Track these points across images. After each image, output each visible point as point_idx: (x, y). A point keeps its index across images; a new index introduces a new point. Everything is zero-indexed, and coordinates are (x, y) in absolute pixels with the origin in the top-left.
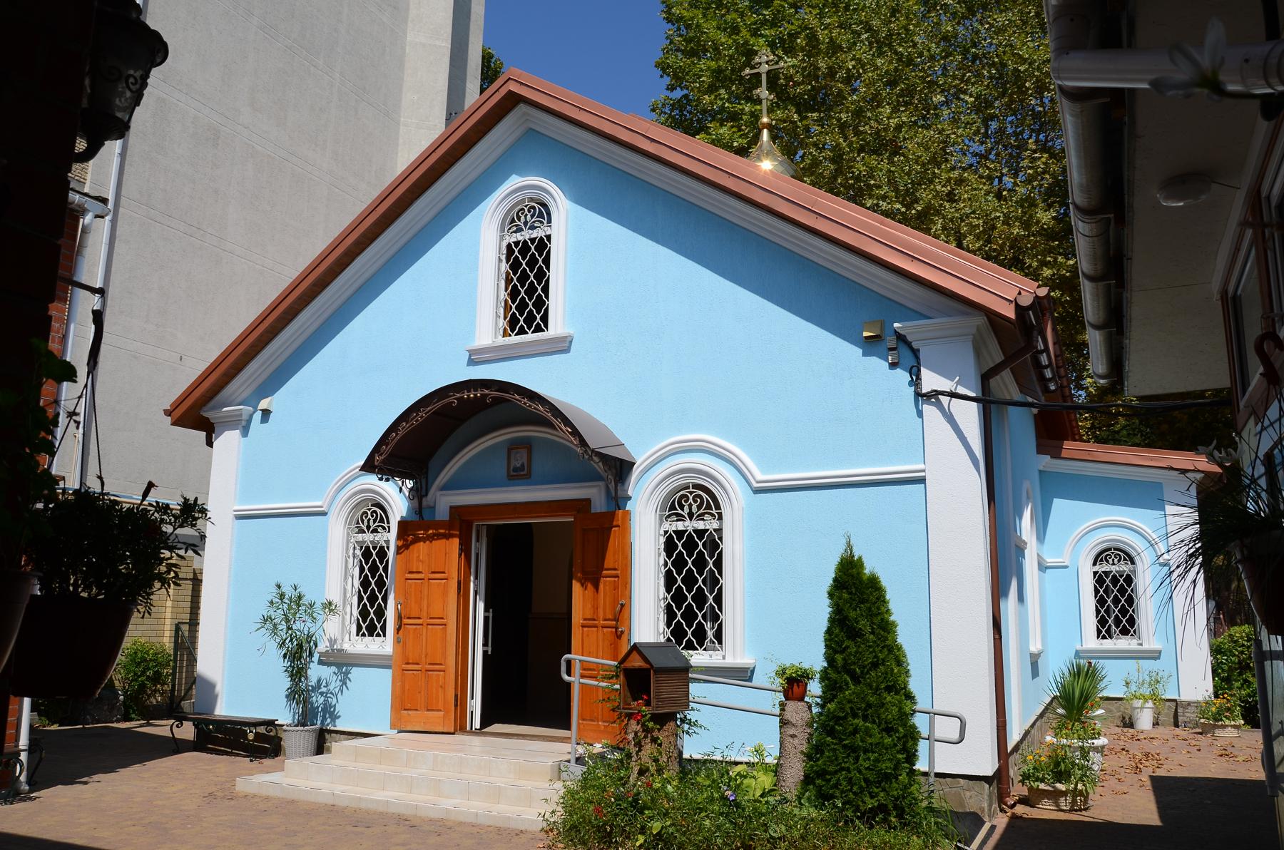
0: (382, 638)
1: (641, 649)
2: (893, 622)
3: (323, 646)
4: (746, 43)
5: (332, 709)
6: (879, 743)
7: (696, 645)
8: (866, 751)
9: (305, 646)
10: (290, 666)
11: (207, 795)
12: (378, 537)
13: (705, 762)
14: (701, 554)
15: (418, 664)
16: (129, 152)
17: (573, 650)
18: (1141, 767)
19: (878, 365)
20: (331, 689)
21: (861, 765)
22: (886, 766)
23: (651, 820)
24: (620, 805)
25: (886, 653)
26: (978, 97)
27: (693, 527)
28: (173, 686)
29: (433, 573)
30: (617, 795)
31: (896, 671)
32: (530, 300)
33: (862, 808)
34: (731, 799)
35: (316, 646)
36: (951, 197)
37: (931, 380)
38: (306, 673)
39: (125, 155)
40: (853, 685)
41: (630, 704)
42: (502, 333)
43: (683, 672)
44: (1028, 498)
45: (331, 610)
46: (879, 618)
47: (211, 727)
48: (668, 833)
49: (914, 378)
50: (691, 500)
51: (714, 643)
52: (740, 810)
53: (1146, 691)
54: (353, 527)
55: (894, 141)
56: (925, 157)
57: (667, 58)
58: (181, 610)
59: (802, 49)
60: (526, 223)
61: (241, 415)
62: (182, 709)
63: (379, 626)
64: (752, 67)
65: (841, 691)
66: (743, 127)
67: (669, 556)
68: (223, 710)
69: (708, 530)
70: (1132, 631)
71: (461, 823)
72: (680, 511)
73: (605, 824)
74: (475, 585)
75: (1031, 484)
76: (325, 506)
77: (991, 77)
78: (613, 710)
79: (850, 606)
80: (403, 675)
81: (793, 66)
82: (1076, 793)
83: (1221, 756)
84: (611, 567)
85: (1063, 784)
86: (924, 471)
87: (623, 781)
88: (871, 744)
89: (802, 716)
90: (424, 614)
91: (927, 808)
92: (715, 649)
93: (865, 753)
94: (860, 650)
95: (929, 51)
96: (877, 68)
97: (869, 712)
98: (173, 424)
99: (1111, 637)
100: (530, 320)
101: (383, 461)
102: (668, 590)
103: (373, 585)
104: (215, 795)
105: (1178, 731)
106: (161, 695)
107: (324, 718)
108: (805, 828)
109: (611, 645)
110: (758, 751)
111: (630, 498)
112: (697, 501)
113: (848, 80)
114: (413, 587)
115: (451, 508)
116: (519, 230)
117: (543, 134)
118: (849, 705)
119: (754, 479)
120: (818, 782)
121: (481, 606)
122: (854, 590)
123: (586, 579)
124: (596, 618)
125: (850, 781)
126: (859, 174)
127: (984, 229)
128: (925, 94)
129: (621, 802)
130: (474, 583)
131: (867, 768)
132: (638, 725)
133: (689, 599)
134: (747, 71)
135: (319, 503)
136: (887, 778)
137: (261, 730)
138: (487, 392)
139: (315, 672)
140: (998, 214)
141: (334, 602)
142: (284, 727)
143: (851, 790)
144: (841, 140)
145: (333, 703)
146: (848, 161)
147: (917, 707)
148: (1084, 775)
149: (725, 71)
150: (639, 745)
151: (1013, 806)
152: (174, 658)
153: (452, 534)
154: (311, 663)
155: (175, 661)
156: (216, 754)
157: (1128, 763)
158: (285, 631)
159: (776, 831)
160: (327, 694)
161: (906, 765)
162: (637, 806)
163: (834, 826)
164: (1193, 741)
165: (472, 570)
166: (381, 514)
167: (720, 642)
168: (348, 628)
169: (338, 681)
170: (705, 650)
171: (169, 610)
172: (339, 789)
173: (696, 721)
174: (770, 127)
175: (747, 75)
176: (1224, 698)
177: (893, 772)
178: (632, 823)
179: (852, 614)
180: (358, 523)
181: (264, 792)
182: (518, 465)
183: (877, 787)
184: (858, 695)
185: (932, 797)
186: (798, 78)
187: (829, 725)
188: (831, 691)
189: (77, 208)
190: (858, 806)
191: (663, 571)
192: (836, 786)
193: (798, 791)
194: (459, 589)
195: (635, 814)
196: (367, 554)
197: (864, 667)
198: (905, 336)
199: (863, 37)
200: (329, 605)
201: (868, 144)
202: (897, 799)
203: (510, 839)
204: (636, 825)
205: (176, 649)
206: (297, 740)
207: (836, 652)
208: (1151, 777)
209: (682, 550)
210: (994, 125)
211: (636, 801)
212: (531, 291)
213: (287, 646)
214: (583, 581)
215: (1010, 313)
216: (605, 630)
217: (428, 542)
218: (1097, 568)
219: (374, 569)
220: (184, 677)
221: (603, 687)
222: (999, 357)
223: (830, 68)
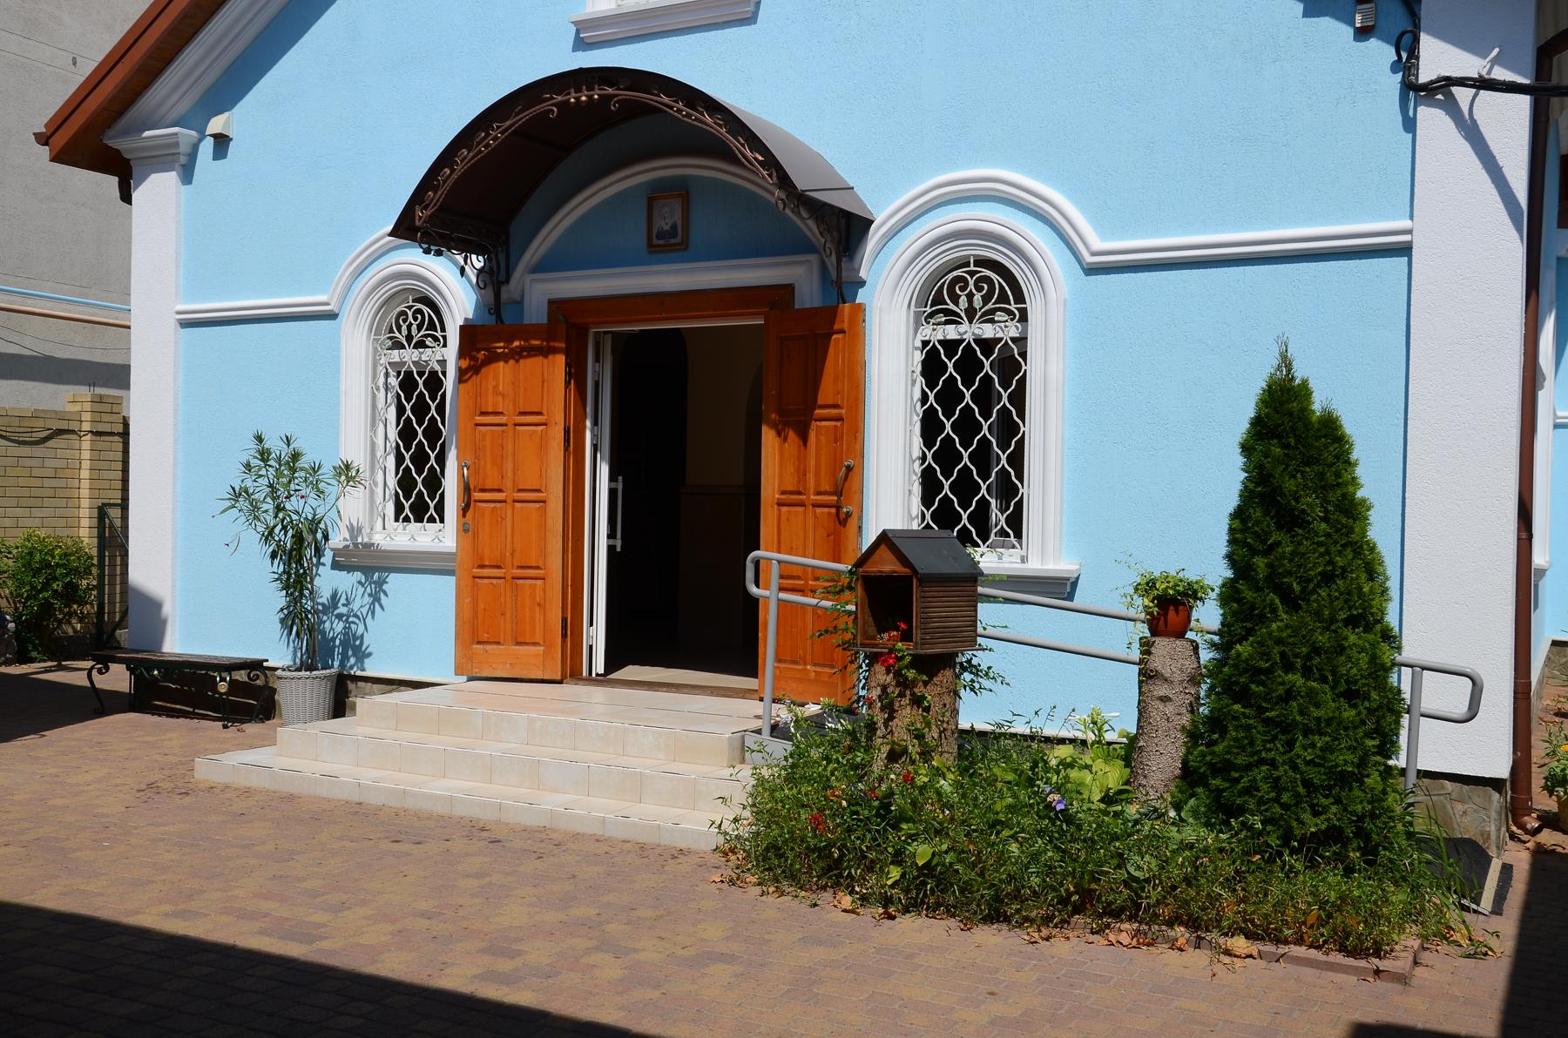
0: (438, 525)
1: (897, 542)
2: (1364, 501)
3: (338, 539)
5: (358, 643)
6: (1333, 718)
7: (976, 538)
8: (1307, 732)
9: (308, 537)
10: (284, 572)
11: (144, 787)
12: (426, 354)
13: (997, 736)
14: (987, 379)
15: (499, 567)
20: (355, 609)
21: (1299, 756)
22: (1345, 759)
23: (913, 841)
24: (857, 813)
25: (1350, 557)
27: (973, 333)
28: (101, 606)
30: (852, 795)
31: (1366, 589)
33: (1298, 832)
34: (1058, 808)
35: (326, 537)
38: (312, 582)
40: (1286, 613)
41: (874, 638)
43: (968, 583)
45: (350, 478)
46: (1339, 492)
47: (156, 672)
48: (944, 865)
49: (1404, 56)
51: (1008, 535)
52: (1073, 829)
54: (382, 338)
58: (106, 484)
61: (177, 145)
62: (118, 642)
63: (432, 505)
67: (931, 384)
68: (176, 644)
71: (577, 837)
73: (831, 844)
74: (594, 436)
79: (1285, 469)
80: (475, 585)
84: (830, 402)
87: (860, 771)
88: (1318, 719)
89: (1182, 665)
90: (509, 484)
93: (1305, 735)
94: (1302, 549)
97: (1315, 662)
101: (430, 219)
103: (420, 436)
104: (158, 787)
106: (81, 620)
107: (345, 658)
109: (828, 536)
110: (1096, 724)
111: (862, 283)
112: (983, 287)
115: (551, 302)
118: (1276, 650)
119: (1087, 247)
120: (1216, 782)
121: (604, 470)
122: (1292, 441)
123: (786, 424)
125: (1276, 784)
129: (859, 808)
130: (592, 431)
131: (1308, 763)
132: (888, 674)
133: (966, 459)
136: (1344, 780)
137: (241, 675)
138: (610, 91)
139: (327, 581)
141: (355, 464)
142: (279, 672)
150: (890, 710)
152: (99, 561)
153: (554, 347)
154: (321, 567)
155: (101, 565)
156: (168, 716)
158: (271, 512)
159: (1139, 868)
160: (348, 617)
161: (1378, 758)
165: (589, 409)
166: (429, 313)
167: (1019, 535)
168: (380, 509)
169: (366, 595)
171: (85, 484)
172: (368, 775)
177: (1356, 771)
178: (879, 845)
179: (1290, 485)
180: (391, 331)
181: (243, 781)
182: (666, 228)
183: (1326, 796)
187: (1237, 683)
188: (1243, 621)
190: (1289, 830)
192: (1248, 791)
196: (408, 383)
197: (1309, 581)
200: (346, 471)
202: (1361, 819)
203: (663, 867)
204: (886, 848)
205: (102, 547)
207: (1254, 552)
209: (955, 374)
211: (886, 807)
213: (276, 538)
214: (780, 427)
216: (819, 510)
217: (512, 362)
219: (421, 409)
221: (826, 609)
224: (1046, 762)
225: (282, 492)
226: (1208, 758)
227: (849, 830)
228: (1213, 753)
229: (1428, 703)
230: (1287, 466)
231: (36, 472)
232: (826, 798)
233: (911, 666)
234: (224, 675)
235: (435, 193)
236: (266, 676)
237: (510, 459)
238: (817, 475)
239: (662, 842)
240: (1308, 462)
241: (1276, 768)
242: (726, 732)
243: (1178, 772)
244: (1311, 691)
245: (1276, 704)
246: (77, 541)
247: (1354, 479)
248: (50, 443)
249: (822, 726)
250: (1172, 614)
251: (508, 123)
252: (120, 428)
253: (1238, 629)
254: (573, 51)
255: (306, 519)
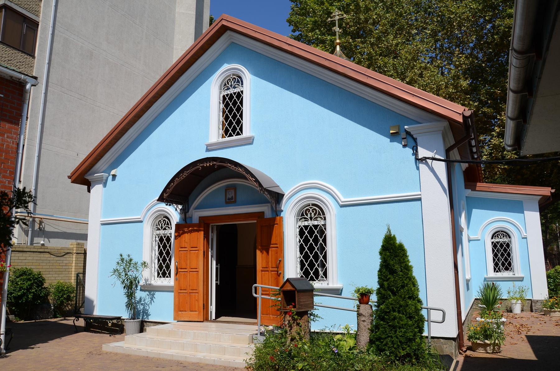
0: (169, 278)
1: (291, 281)
3: (142, 283)
4: (327, 9)
5: (147, 312)
6: (406, 324)
8: (400, 328)
9: (134, 282)
10: (127, 292)
11: (88, 353)
12: (166, 232)
14: (316, 236)
15: (186, 290)
16: (52, 62)
17: (257, 283)
18: (520, 331)
19: (397, 146)
20: (146, 302)
21: (398, 335)
22: (410, 335)
24: (282, 356)
25: (408, 281)
26: (432, 30)
28: (76, 302)
29: (192, 248)
31: (413, 289)
32: (234, 121)
33: (399, 355)
34: (336, 352)
35: (139, 282)
36: (421, 75)
37: (423, 153)
38: (134, 295)
39: (50, 64)
41: (286, 307)
42: (221, 136)
43: (311, 292)
44: (463, 208)
45: (145, 266)
48: (306, 369)
49: (415, 152)
50: (311, 211)
52: (340, 357)
53: (518, 296)
54: (155, 227)
55: (395, 51)
56: (410, 57)
57: (292, 18)
58: (79, 267)
59: (353, 11)
60: (231, 86)
61: (103, 177)
62: (81, 312)
63: (167, 273)
64: (331, 18)
65: (387, 299)
66: (327, 46)
67: (301, 237)
68: (97, 312)
69: (319, 225)
70: (510, 268)
71: (207, 365)
72: (306, 217)
73: (275, 365)
74: (211, 253)
75: (463, 202)
76: (142, 218)
77: (438, 21)
78: (278, 310)
80: (179, 295)
81: (349, 19)
82: (494, 344)
83: (557, 325)
85: (488, 340)
86: (420, 195)
88: (402, 324)
90: (188, 267)
91: (428, 354)
92: (323, 280)
93: (399, 329)
94: (396, 279)
95: (409, 10)
96: (387, 18)
97: (401, 309)
98: (72, 182)
99: (500, 271)
100: (234, 130)
101: (168, 197)
102: (301, 253)
103: (164, 254)
105: (533, 314)
106: (71, 306)
107: (143, 316)
108: (372, 365)
110: (347, 328)
111: (282, 211)
113: (374, 24)
114: (183, 254)
115: (200, 217)
116: (228, 89)
117: (238, 44)
118: (391, 306)
120: (377, 343)
121: (214, 263)
122: (392, 251)
123: (263, 249)
124: (197, 289)
125: (393, 342)
126: (380, 66)
127: (437, 90)
128: (408, 30)
130: (211, 252)
131: (401, 336)
132: (290, 317)
134: (329, 19)
135: (139, 217)
136: (410, 340)
138: (215, 163)
139: (139, 294)
140: (443, 83)
141: (147, 262)
142: (125, 320)
143: (393, 347)
144: (372, 50)
145: (147, 309)
146: (375, 60)
147: (423, 306)
148: (498, 336)
149: (318, 22)
150: (291, 327)
151: (465, 351)
155: (77, 290)
156: (94, 333)
157: (514, 329)
158: (124, 276)
159: (358, 367)
160: (144, 304)
161: (419, 334)
162: (291, 356)
163: (385, 364)
164: (541, 318)
167: (326, 277)
170: (319, 281)
171: (74, 267)
173: (317, 315)
174: (339, 44)
175: (329, 21)
176: (554, 298)
178: (289, 364)
179: (392, 263)
181: (115, 351)
182: (230, 197)
183: (406, 345)
184: (395, 301)
185: (430, 349)
186: (351, 24)
187: (381, 316)
189: (23, 82)
191: (299, 244)
192: (386, 345)
193: (367, 347)
194: (204, 255)
195: (290, 360)
196: (161, 240)
198: (410, 132)
199: (380, 5)
200: (144, 264)
201: (383, 52)
202: (415, 350)
205: (77, 285)
206: (131, 326)
207: (384, 281)
208: (526, 336)
210: (439, 43)
211: (290, 354)
212: (234, 117)
215: (460, 119)
216: (272, 272)
217: (189, 234)
218: (493, 240)
219: (165, 247)
220: (81, 297)
222: (452, 142)
223: (366, 18)
224: (333, 340)
225: (127, 270)
226: (375, 336)
227: (281, 361)
228: (376, 335)
229: (433, 318)
230: (391, 258)
231: (61, 264)
232: (274, 352)
233: (296, 314)
234: (110, 321)
235: (169, 190)
236: (122, 321)
237: (189, 260)
238: (272, 263)
239: (231, 366)
240: (396, 256)
241: (392, 338)
242: (248, 335)
243: (368, 341)
244: (400, 317)
245: (392, 321)
246: (71, 283)
247: (408, 260)
248: (65, 256)
249: (273, 332)
250: (364, 298)
251: (188, 171)
252: (83, 252)
253: (381, 301)
254: (206, 152)
255: (133, 277)
